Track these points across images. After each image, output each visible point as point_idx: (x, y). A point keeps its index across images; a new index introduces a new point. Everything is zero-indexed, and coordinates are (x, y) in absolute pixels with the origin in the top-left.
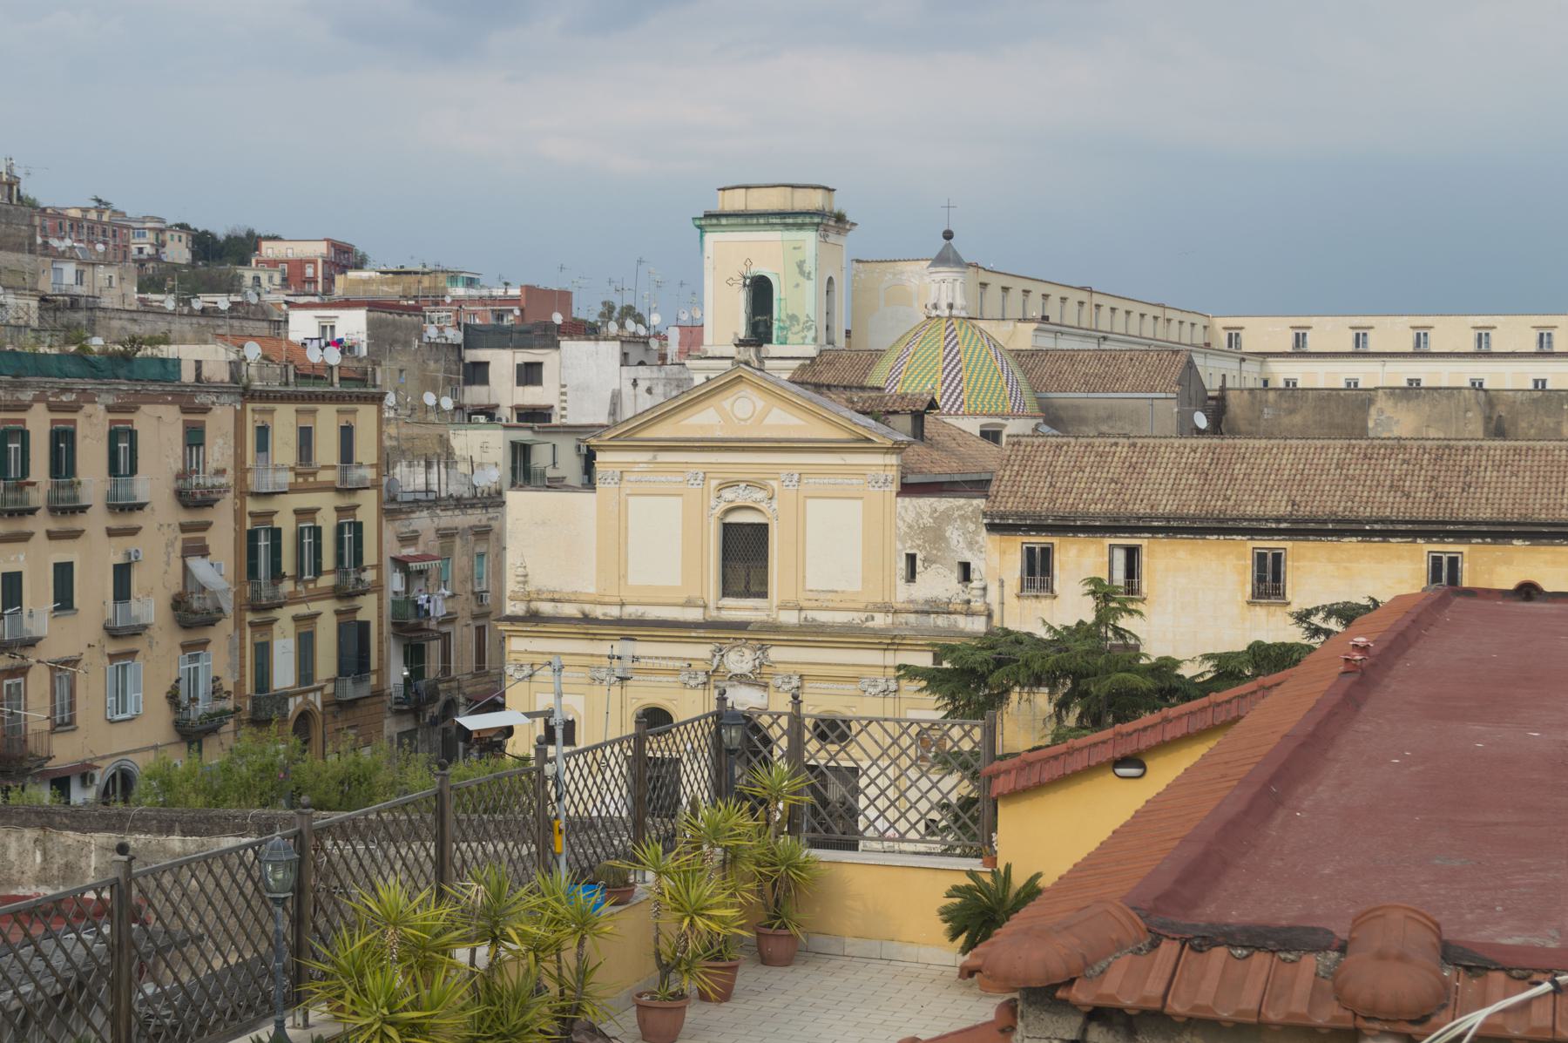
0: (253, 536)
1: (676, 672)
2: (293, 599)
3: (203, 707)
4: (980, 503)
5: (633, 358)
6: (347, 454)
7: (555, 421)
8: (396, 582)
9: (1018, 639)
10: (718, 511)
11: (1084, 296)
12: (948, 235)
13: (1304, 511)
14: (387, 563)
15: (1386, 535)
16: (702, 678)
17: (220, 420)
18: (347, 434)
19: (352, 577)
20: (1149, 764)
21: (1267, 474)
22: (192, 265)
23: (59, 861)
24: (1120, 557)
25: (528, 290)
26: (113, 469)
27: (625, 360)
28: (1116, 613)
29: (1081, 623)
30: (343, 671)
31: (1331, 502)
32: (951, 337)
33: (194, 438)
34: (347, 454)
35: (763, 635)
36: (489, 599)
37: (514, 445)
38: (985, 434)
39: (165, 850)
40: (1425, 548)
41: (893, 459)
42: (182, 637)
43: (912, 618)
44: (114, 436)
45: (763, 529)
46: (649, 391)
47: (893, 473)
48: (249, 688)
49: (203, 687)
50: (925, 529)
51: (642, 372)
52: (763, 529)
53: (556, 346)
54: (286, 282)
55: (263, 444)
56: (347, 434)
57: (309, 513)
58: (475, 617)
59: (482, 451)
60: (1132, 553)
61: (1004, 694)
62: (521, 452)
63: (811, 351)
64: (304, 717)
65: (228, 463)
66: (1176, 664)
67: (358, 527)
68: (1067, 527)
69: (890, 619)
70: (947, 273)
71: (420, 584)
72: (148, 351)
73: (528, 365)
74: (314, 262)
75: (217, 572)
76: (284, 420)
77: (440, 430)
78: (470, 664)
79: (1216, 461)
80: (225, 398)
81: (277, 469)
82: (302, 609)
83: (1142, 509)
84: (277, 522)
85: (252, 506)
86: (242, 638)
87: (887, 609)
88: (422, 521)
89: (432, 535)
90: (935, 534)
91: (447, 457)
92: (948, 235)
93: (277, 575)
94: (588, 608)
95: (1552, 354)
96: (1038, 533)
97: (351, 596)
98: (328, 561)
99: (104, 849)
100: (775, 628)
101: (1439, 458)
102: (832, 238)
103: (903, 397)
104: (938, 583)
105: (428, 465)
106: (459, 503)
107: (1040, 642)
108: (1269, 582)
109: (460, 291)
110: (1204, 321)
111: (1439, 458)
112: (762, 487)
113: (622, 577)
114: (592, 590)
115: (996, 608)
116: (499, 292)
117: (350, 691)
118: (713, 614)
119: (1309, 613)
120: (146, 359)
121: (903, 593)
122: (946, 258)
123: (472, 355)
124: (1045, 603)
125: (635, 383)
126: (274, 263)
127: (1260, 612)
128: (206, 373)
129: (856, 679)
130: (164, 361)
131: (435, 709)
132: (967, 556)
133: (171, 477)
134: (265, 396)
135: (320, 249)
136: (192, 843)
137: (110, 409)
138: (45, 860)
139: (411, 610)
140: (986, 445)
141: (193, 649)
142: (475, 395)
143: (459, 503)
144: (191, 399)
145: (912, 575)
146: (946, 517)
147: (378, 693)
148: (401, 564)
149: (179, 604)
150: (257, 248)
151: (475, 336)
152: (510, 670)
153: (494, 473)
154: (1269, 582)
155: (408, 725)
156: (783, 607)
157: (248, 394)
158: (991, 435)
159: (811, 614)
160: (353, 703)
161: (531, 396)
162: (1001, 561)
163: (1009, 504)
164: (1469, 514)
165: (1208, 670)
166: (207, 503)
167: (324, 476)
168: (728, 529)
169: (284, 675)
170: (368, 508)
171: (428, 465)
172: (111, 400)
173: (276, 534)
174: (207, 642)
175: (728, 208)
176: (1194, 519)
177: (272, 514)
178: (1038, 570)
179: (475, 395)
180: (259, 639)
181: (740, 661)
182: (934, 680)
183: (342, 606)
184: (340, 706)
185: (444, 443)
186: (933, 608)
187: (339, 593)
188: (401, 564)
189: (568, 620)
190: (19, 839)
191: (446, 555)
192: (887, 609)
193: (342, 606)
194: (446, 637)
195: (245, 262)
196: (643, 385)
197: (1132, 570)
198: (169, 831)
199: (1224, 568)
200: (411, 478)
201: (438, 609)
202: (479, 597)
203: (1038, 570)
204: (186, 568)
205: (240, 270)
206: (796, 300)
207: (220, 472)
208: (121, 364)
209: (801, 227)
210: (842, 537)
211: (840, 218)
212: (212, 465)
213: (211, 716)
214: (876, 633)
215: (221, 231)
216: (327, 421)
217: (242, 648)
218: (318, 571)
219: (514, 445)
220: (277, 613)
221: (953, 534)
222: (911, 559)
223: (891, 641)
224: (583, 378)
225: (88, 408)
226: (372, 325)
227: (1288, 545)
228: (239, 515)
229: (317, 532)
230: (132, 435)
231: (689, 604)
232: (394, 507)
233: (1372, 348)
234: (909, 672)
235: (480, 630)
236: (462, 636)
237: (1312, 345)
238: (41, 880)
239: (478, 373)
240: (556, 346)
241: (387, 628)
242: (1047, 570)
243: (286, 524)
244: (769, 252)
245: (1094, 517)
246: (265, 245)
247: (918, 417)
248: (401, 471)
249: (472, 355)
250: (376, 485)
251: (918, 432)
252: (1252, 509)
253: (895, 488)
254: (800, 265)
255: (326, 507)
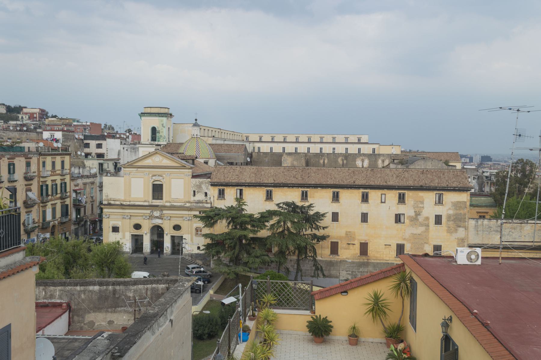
0: (42, 186)
1: (143, 216)
2: (51, 200)
3: (30, 226)
4: (209, 180)
5: (123, 143)
6: (63, 167)
7: (105, 158)
8: (74, 195)
9: (220, 209)
10: (152, 181)
11: (219, 130)
12: (196, 120)
13: (276, 182)
14: (72, 191)
15: (293, 187)
16: (148, 217)
17: (34, 161)
18: (63, 162)
19: (64, 195)
20: (349, 292)
21: (269, 174)
22: (7, 113)
23: (49, 294)
24: (238, 191)
25: (91, 123)
26: (9, 173)
27: (121, 143)
28: (242, 205)
29: (232, 206)
30: (62, 215)
31: (282, 180)
32: (197, 141)
33: (28, 165)
34: (63, 167)
35: (162, 208)
36: (94, 198)
37: (99, 164)
38: (205, 162)
39: (76, 290)
40: (301, 189)
41: (191, 171)
42: (26, 210)
43: (195, 204)
44: (9, 165)
45: (162, 185)
46: (127, 150)
47: (191, 174)
48: (41, 221)
49: (31, 221)
50: (197, 185)
51: (125, 146)
52: (162, 185)
53: (106, 140)
54: (29, 118)
55: (44, 165)
56: (63, 162)
57: (55, 180)
58: (91, 202)
59: (92, 165)
60: (241, 191)
61: (216, 221)
62: (101, 165)
63: (165, 143)
64: (54, 226)
65: (36, 170)
66: (254, 215)
67: (65, 183)
68: (228, 185)
69: (190, 204)
70: (197, 128)
71: (79, 195)
72: (17, 145)
73: (99, 144)
74: (36, 114)
75: (34, 195)
76: (49, 160)
77: (82, 160)
78: (90, 212)
79: (258, 171)
80: (35, 155)
81: (47, 171)
82: (53, 202)
83: (243, 181)
84: (47, 183)
85: (42, 179)
86: (40, 210)
87: (189, 202)
88: (80, 181)
89: (82, 184)
90: (199, 187)
91: (84, 167)
92: (196, 120)
93: (47, 195)
94: (122, 202)
95: (311, 142)
96: (222, 187)
97: (64, 199)
98: (59, 191)
99: (60, 290)
100: (165, 207)
101: (303, 171)
102: (169, 119)
103: (190, 156)
104: (200, 197)
105: (79, 168)
106: (88, 177)
107: (224, 210)
108: (269, 197)
109: (75, 123)
110: (241, 135)
111: (303, 171)
112: (162, 176)
113: (130, 196)
114: (123, 198)
115: (212, 202)
116: (84, 124)
117: (64, 220)
118: (151, 203)
119: (279, 204)
120: (16, 147)
121: (192, 199)
122: (196, 125)
123: (86, 142)
124: (223, 201)
125: (124, 148)
126: (26, 114)
127: (267, 202)
128: (31, 150)
129: (183, 217)
130: (21, 147)
131: (83, 223)
132: (206, 191)
133: (23, 174)
134: (45, 155)
135: (37, 111)
136: (82, 288)
137: (8, 159)
138: (45, 293)
139: (77, 201)
140: (205, 165)
141: (28, 213)
142: (87, 150)
143: (88, 177)
144: (27, 155)
145: (194, 195)
146: (202, 183)
147: (70, 220)
148: (75, 191)
149: (25, 203)
150: (22, 110)
151: (86, 137)
152: (104, 216)
153: (95, 170)
154: (269, 197)
155: (77, 227)
156: (166, 202)
157: (40, 154)
158: (206, 163)
159: (172, 203)
160: (65, 223)
161: (100, 151)
162: (213, 192)
163: (215, 180)
164: (310, 183)
165: (259, 216)
166: (31, 179)
167: (58, 172)
168: (153, 185)
169: (49, 217)
170: (67, 179)
171: (79, 168)
172: (8, 157)
173: (47, 186)
174: (31, 211)
175: (146, 112)
176: (254, 183)
177: (46, 181)
178: (221, 194)
179: (87, 150)
180: (43, 209)
181: (157, 213)
182: (202, 219)
183: (62, 201)
184: (62, 223)
185: (83, 163)
186: (199, 202)
187: (62, 198)
188: (75, 191)
189: (117, 205)
190: (39, 289)
191: (85, 189)
192: (189, 202)
193: (62, 201)
194: (85, 207)
195: (19, 113)
196: (125, 149)
197: (241, 194)
198: (77, 285)
199: (261, 193)
200: (76, 171)
201: (84, 201)
202: (92, 197)
203: (221, 194)
204: (26, 194)
205: (18, 115)
206: (163, 133)
207: (34, 172)
208: (10, 148)
209: (163, 116)
210: (179, 187)
211: (171, 115)
212: (32, 171)
213: (33, 228)
214: (187, 207)
215: (13, 105)
216: (58, 159)
217: (40, 212)
218: (57, 194)
219: (99, 164)
220: (47, 203)
221: (203, 186)
222: (194, 192)
223: (190, 209)
224: (112, 147)
225: (3, 159)
226: (63, 135)
227: (273, 189)
228: (39, 182)
229: (56, 185)
230: (14, 165)
231: (145, 201)
232: (73, 178)
233: (275, 141)
234: (195, 216)
235: (92, 205)
236: (89, 206)
237: (263, 140)
238: (44, 298)
239: (87, 146)
240: (106, 140)
241: (72, 205)
242: (223, 194)
243: (49, 183)
244: (155, 122)
245: (233, 183)
246: (24, 109)
247: (193, 160)
248: (73, 169)
249: (86, 142)
250: (69, 174)
251: (193, 164)
252: (266, 181)
253: (191, 176)
254: (163, 125)
255: (58, 179)
